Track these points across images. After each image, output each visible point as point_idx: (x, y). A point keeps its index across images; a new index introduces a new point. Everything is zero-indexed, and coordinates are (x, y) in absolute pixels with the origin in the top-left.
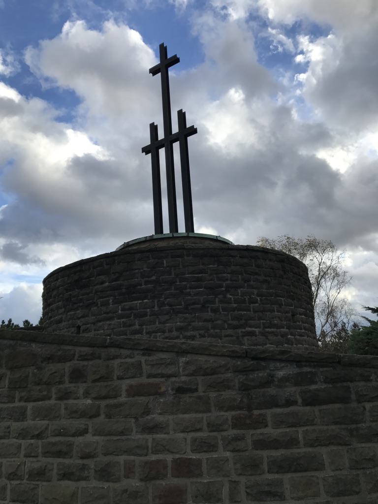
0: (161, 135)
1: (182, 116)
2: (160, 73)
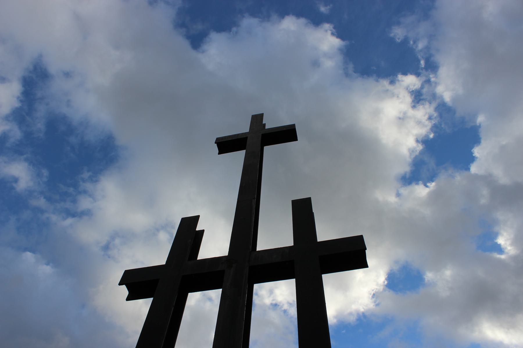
0: (215, 244)
1: (303, 214)
2: (152, 299)
